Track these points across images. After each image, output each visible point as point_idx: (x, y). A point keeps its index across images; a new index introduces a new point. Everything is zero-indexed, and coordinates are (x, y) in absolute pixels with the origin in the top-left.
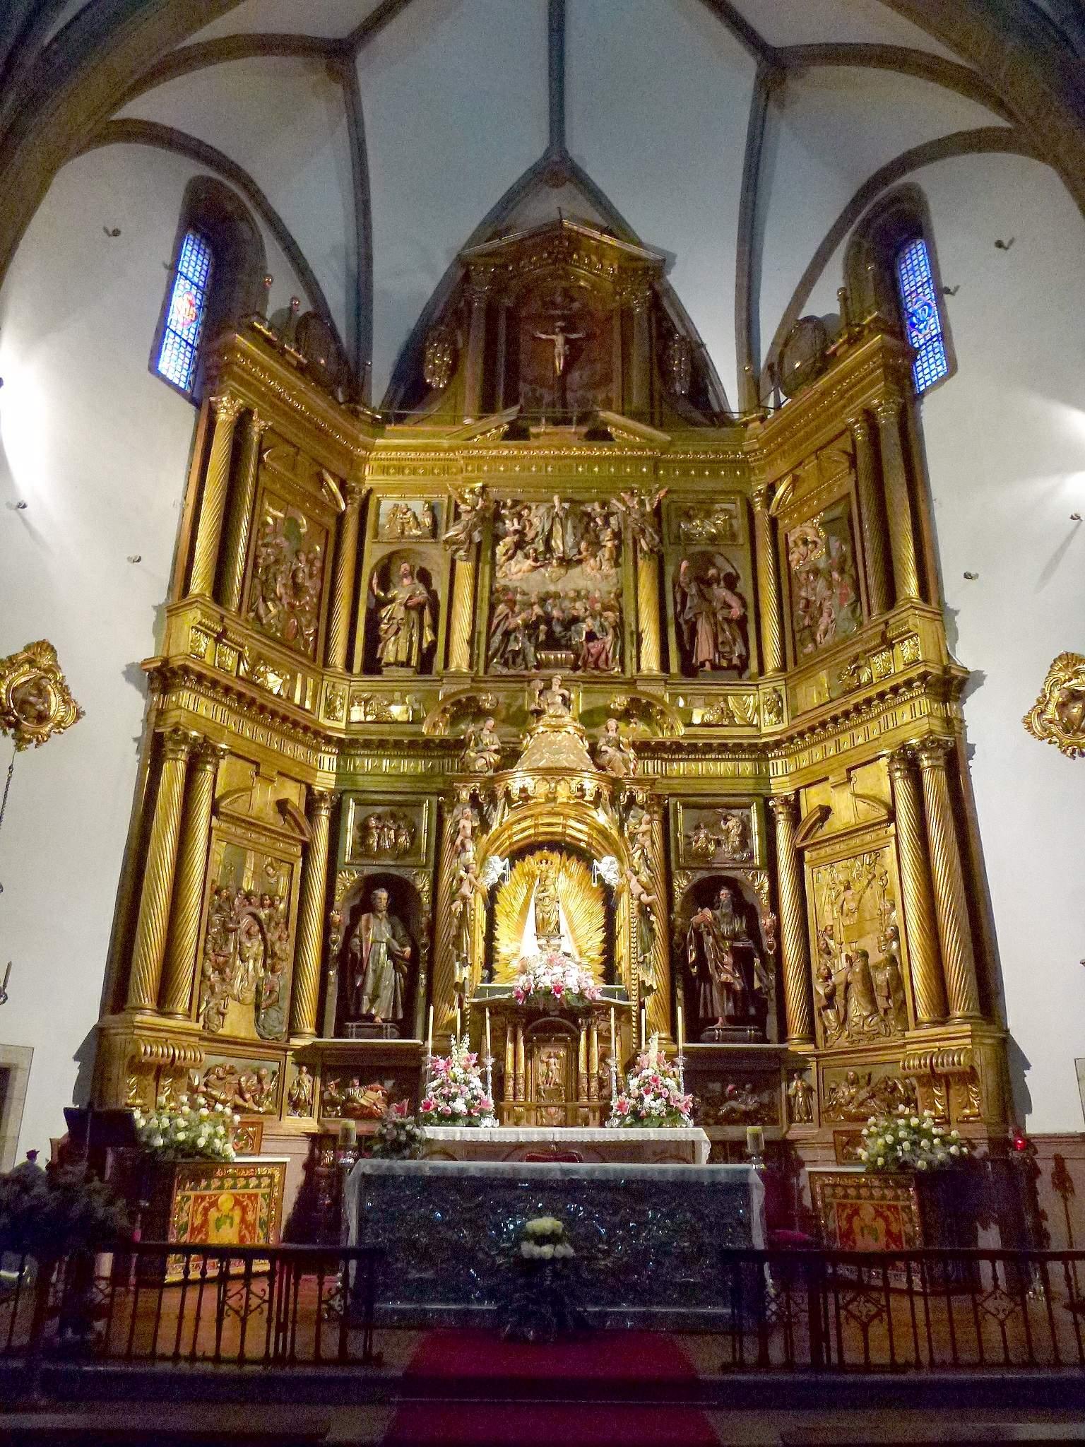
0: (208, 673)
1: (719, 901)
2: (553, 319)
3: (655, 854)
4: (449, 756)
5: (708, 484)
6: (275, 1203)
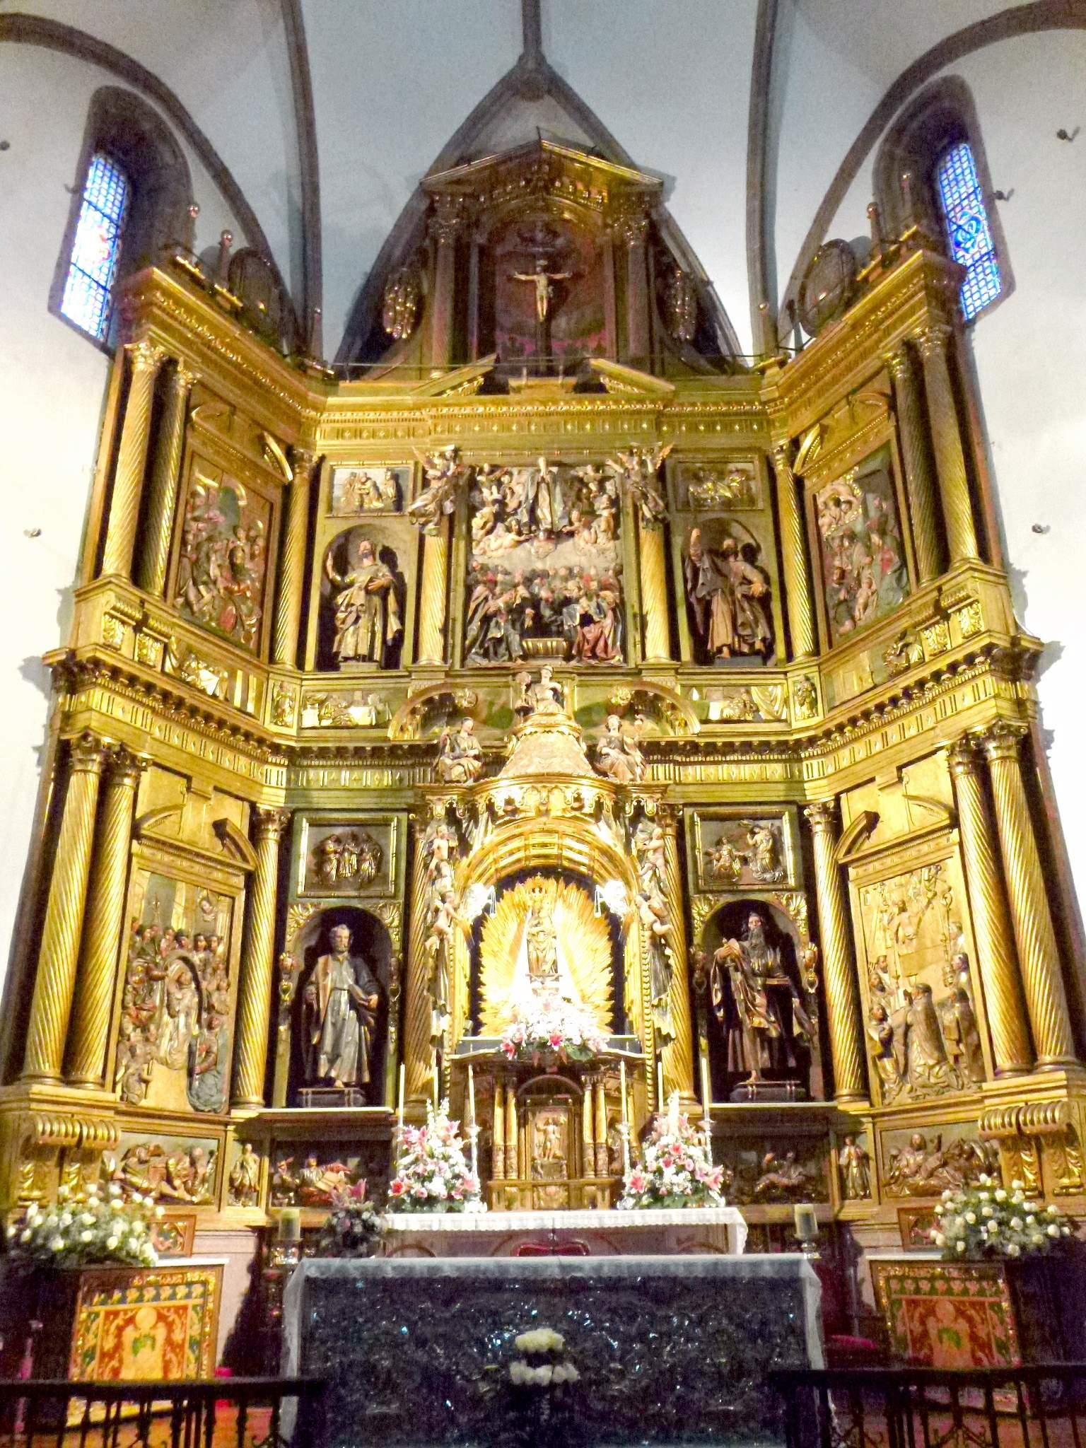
0: (125, 668)
1: (748, 929)
2: (534, 257)
3: (670, 875)
4: (421, 765)
5: (719, 440)
6: (209, 1316)
